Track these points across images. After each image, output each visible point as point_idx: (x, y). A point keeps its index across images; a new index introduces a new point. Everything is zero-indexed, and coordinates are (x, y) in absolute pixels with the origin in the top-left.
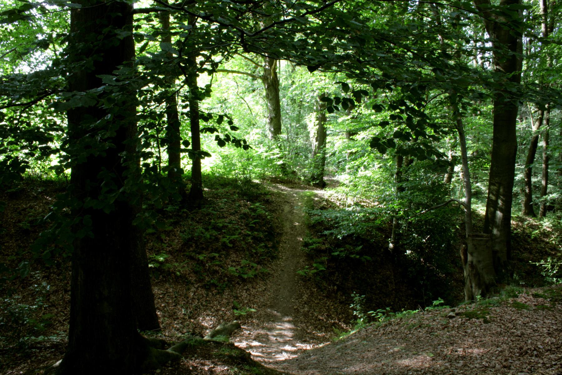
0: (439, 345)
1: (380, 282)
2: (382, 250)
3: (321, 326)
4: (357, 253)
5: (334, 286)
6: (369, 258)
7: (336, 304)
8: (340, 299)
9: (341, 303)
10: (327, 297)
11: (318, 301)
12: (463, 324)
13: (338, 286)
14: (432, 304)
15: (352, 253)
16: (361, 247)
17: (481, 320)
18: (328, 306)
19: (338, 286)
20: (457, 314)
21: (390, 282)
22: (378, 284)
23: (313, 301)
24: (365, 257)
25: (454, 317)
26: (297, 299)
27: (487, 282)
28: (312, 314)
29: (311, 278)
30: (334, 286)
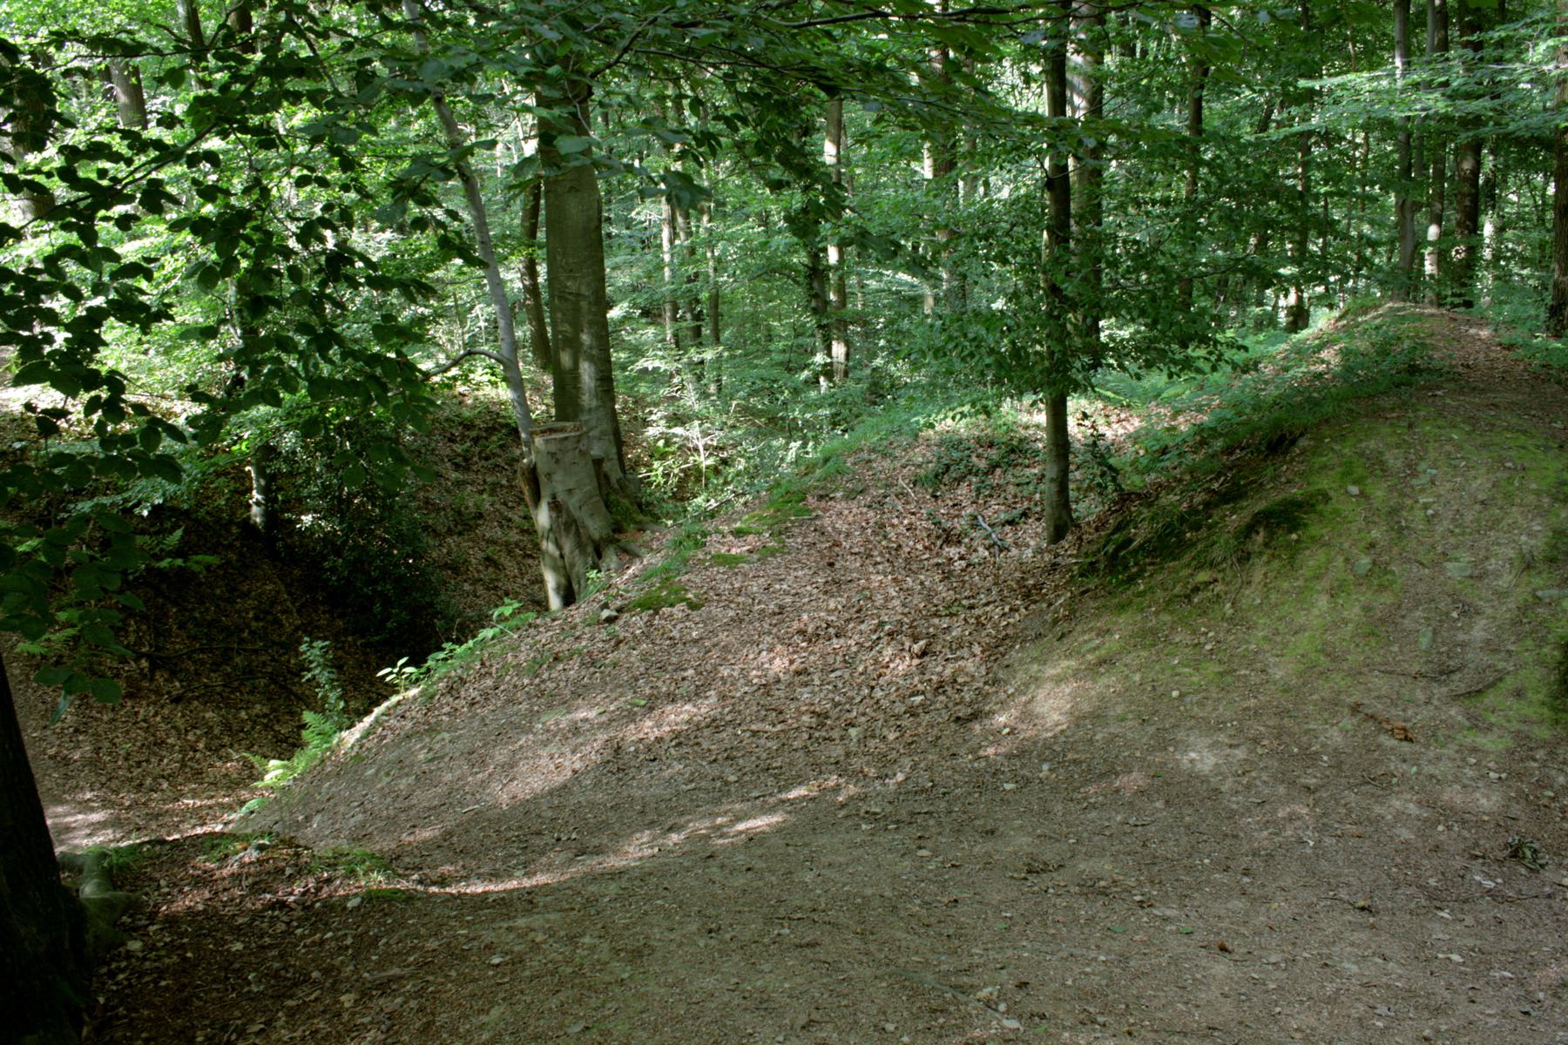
0: (637, 680)
1: (257, 618)
2: (235, 530)
3: (154, 779)
4: (178, 552)
5: (137, 660)
6: (209, 559)
7: (162, 707)
8: (169, 693)
9: (177, 700)
10: (130, 696)
11: (111, 715)
12: (649, 624)
13: (148, 656)
14: (489, 617)
15: (159, 558)
16: (179, 533)
17: (682, 606)
18: (145, 721)
19: (148, 656)
20: (620, 610)
21: (284, 612)
22: (254, 624)
23: (96, 719)
24: (199, 557)
25: (616, 618)
26: (45, 727)
27: (596, 536)
28: (110, 754)
29: (61, 656)
30: (137, 660)
